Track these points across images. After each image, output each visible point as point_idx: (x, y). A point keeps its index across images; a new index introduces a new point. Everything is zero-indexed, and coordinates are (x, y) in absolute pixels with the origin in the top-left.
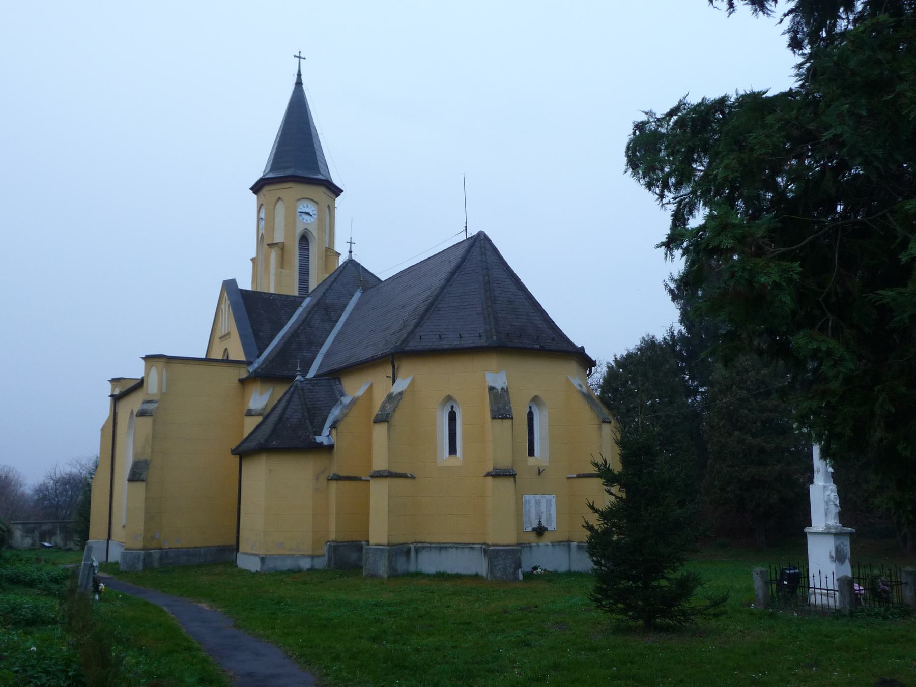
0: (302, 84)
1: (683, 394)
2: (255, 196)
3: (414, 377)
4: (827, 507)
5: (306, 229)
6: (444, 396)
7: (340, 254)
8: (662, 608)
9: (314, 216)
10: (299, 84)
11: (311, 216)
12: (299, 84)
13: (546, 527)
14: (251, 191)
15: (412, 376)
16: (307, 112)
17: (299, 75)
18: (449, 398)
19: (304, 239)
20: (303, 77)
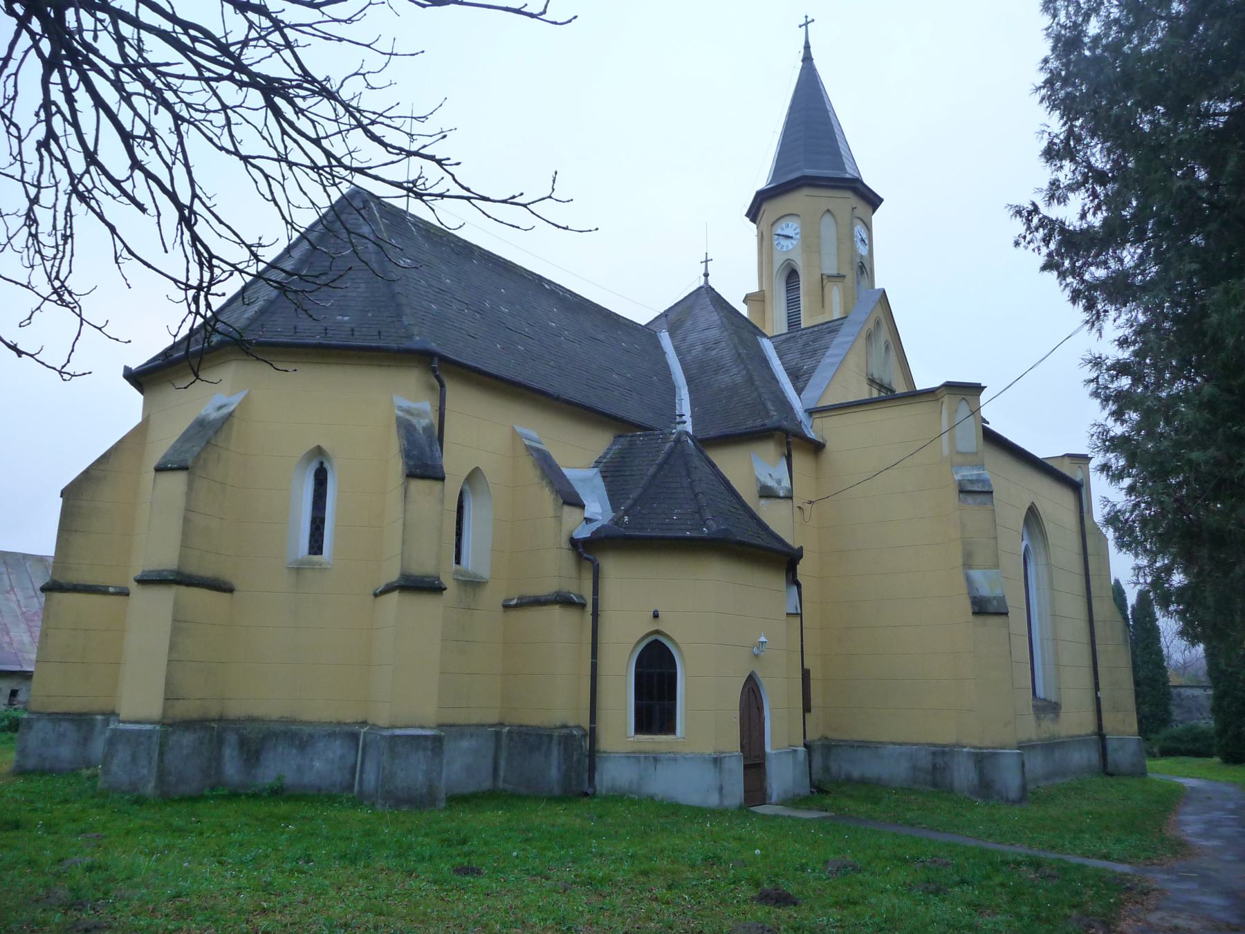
0: (812, 59)
1: (1239, 613)
2: (754, 226)
3: (249, 392)
4: (652, 759)
5: (788, 260)
6: (304, 452)
7: (977, 389)
8: (1168, 395)
9: (798, 236)
10: (807, 59)
11: (792, 238)
12: (807, 59)
13: (997, 592)
14: (747, 219)
15: (246, 392)
16: (826, 111)
17: (807, 47)
18: (319, 451)
19: (792, 276)
20: (812, 50)
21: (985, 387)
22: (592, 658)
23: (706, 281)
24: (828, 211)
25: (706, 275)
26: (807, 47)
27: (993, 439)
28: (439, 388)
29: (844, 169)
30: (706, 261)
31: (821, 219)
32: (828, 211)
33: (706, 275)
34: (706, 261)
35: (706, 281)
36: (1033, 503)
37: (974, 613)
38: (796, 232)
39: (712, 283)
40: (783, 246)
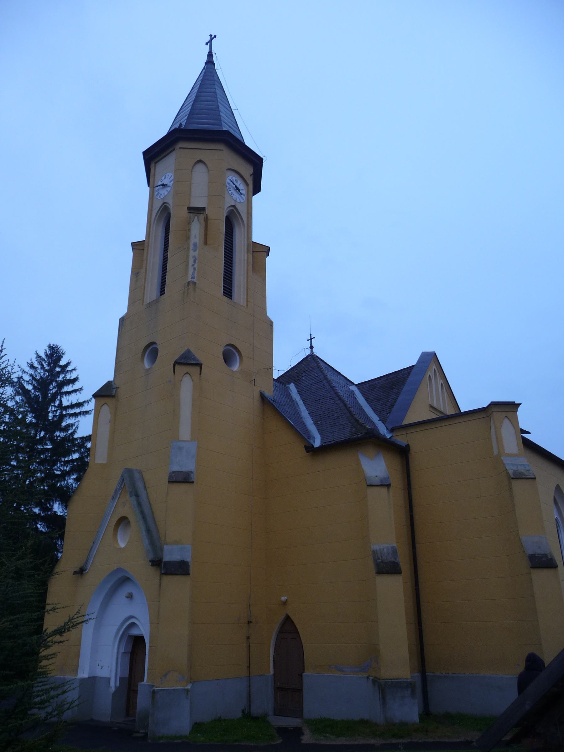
5: (164, 203)
10: (210, 62)
12: (210, 62)
21: (521, 404)
22: (413, 515)
23: (312, 351)
24: (506, 416)
25: (312, 347)
26: (210, 55)
27: (530, 446)
28: (179, 362)
29: (219, 119)
30: (311, 339)
31: (193, 167)
32: (506, 416)
33: (312, 347)
34: (311, 339)
35: (312, 351)
36: (231, 299)
37: (376, 573)
38: (171, 179)
39: (316, 352)
40: (161, 194)
